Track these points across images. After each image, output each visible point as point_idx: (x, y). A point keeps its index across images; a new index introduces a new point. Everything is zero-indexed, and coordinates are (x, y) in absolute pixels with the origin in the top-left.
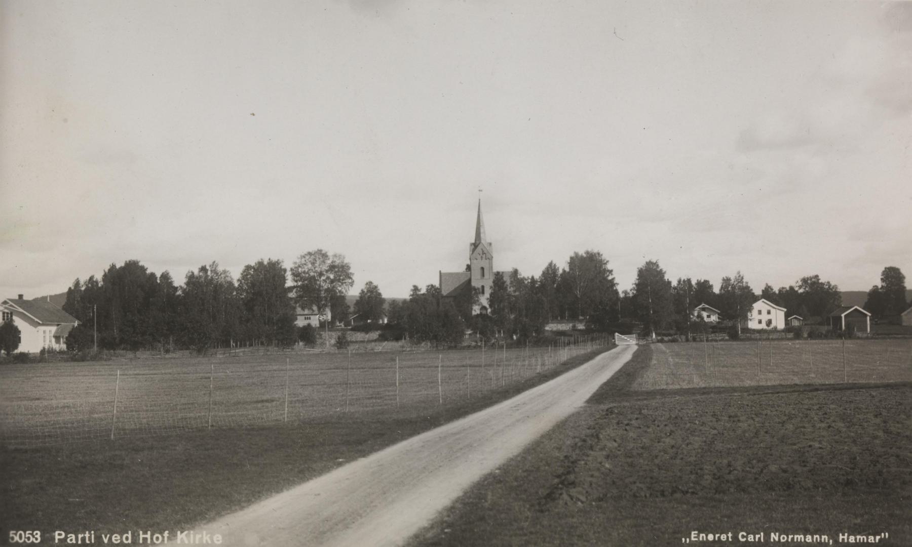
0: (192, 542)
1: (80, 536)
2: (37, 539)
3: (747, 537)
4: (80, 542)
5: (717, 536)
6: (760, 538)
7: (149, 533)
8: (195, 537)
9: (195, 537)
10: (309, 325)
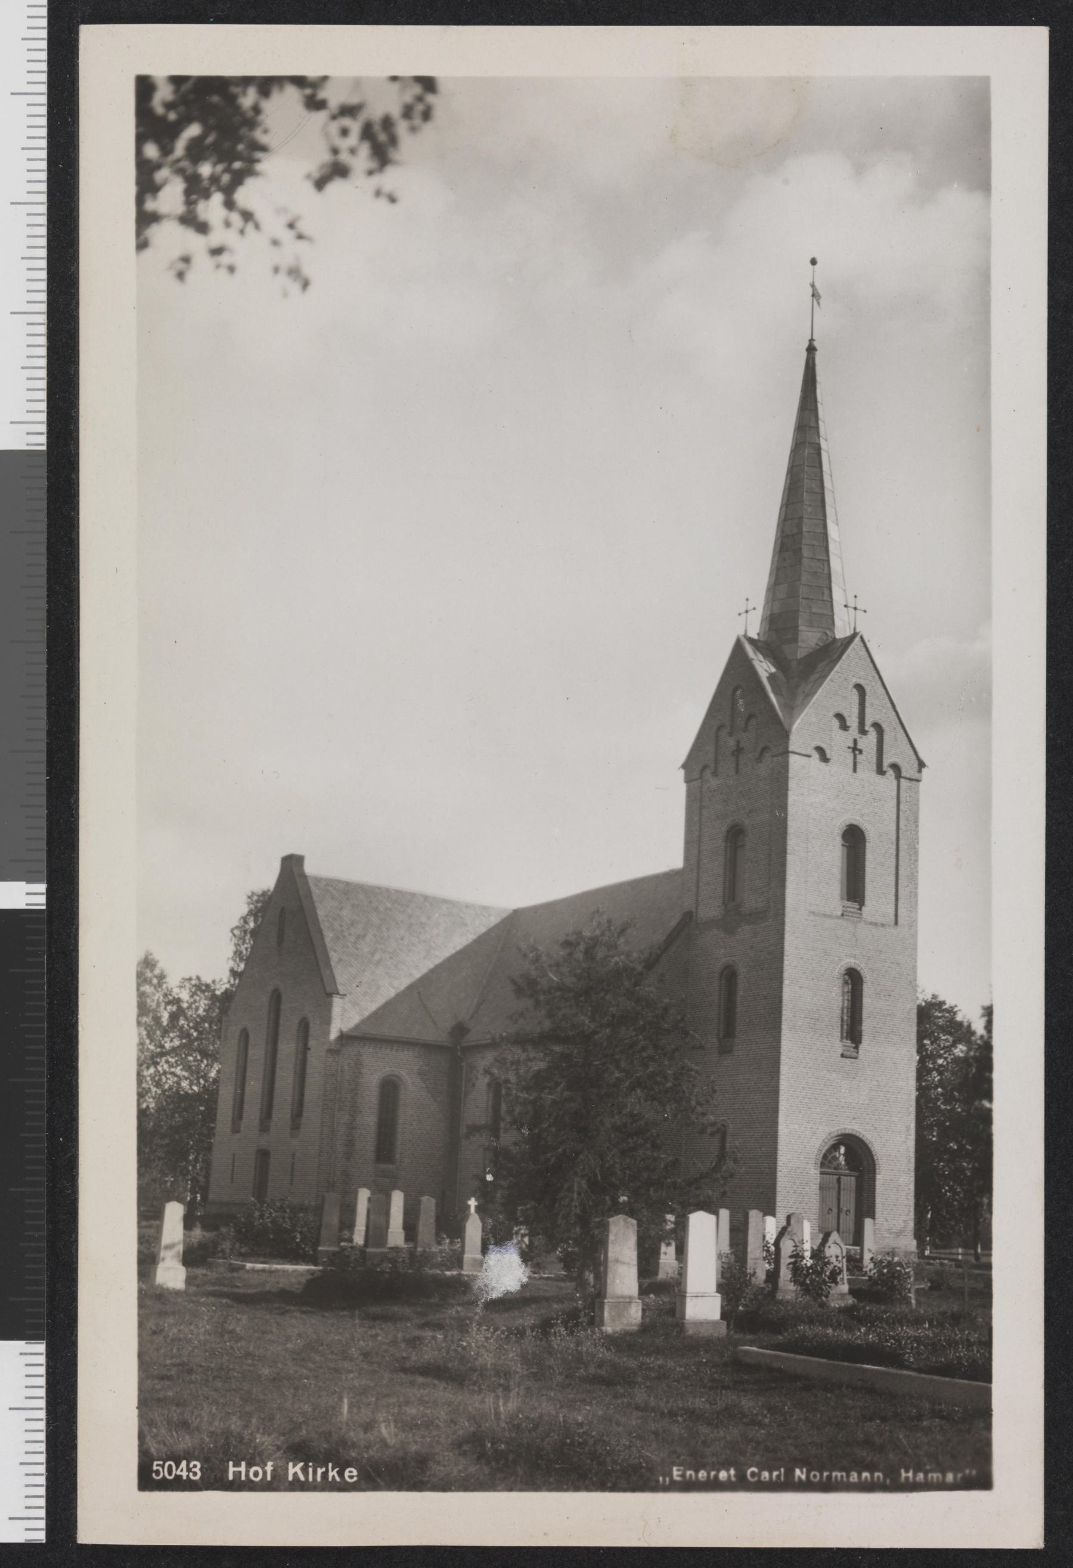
0: (311, 1479)
1: (320, 1471)
2: (195, 1474)
3: (759, 1475)
4: (319, 1479)
5: (713, 1473)
6: (778, 1477)
7: (243, 1464)
8: (315, 1473)
9: (315, 1473)
10: (460, 1274)
